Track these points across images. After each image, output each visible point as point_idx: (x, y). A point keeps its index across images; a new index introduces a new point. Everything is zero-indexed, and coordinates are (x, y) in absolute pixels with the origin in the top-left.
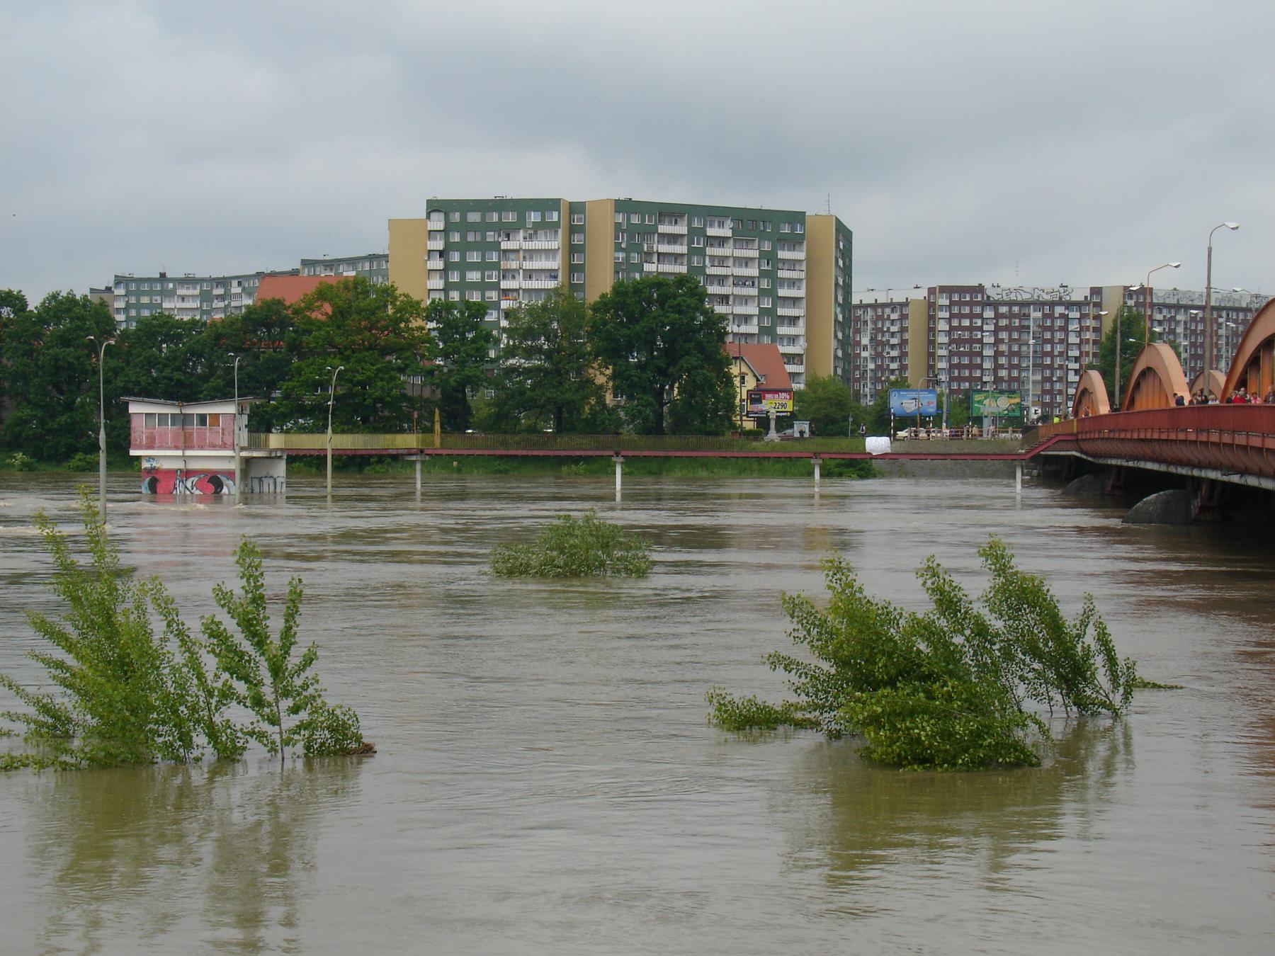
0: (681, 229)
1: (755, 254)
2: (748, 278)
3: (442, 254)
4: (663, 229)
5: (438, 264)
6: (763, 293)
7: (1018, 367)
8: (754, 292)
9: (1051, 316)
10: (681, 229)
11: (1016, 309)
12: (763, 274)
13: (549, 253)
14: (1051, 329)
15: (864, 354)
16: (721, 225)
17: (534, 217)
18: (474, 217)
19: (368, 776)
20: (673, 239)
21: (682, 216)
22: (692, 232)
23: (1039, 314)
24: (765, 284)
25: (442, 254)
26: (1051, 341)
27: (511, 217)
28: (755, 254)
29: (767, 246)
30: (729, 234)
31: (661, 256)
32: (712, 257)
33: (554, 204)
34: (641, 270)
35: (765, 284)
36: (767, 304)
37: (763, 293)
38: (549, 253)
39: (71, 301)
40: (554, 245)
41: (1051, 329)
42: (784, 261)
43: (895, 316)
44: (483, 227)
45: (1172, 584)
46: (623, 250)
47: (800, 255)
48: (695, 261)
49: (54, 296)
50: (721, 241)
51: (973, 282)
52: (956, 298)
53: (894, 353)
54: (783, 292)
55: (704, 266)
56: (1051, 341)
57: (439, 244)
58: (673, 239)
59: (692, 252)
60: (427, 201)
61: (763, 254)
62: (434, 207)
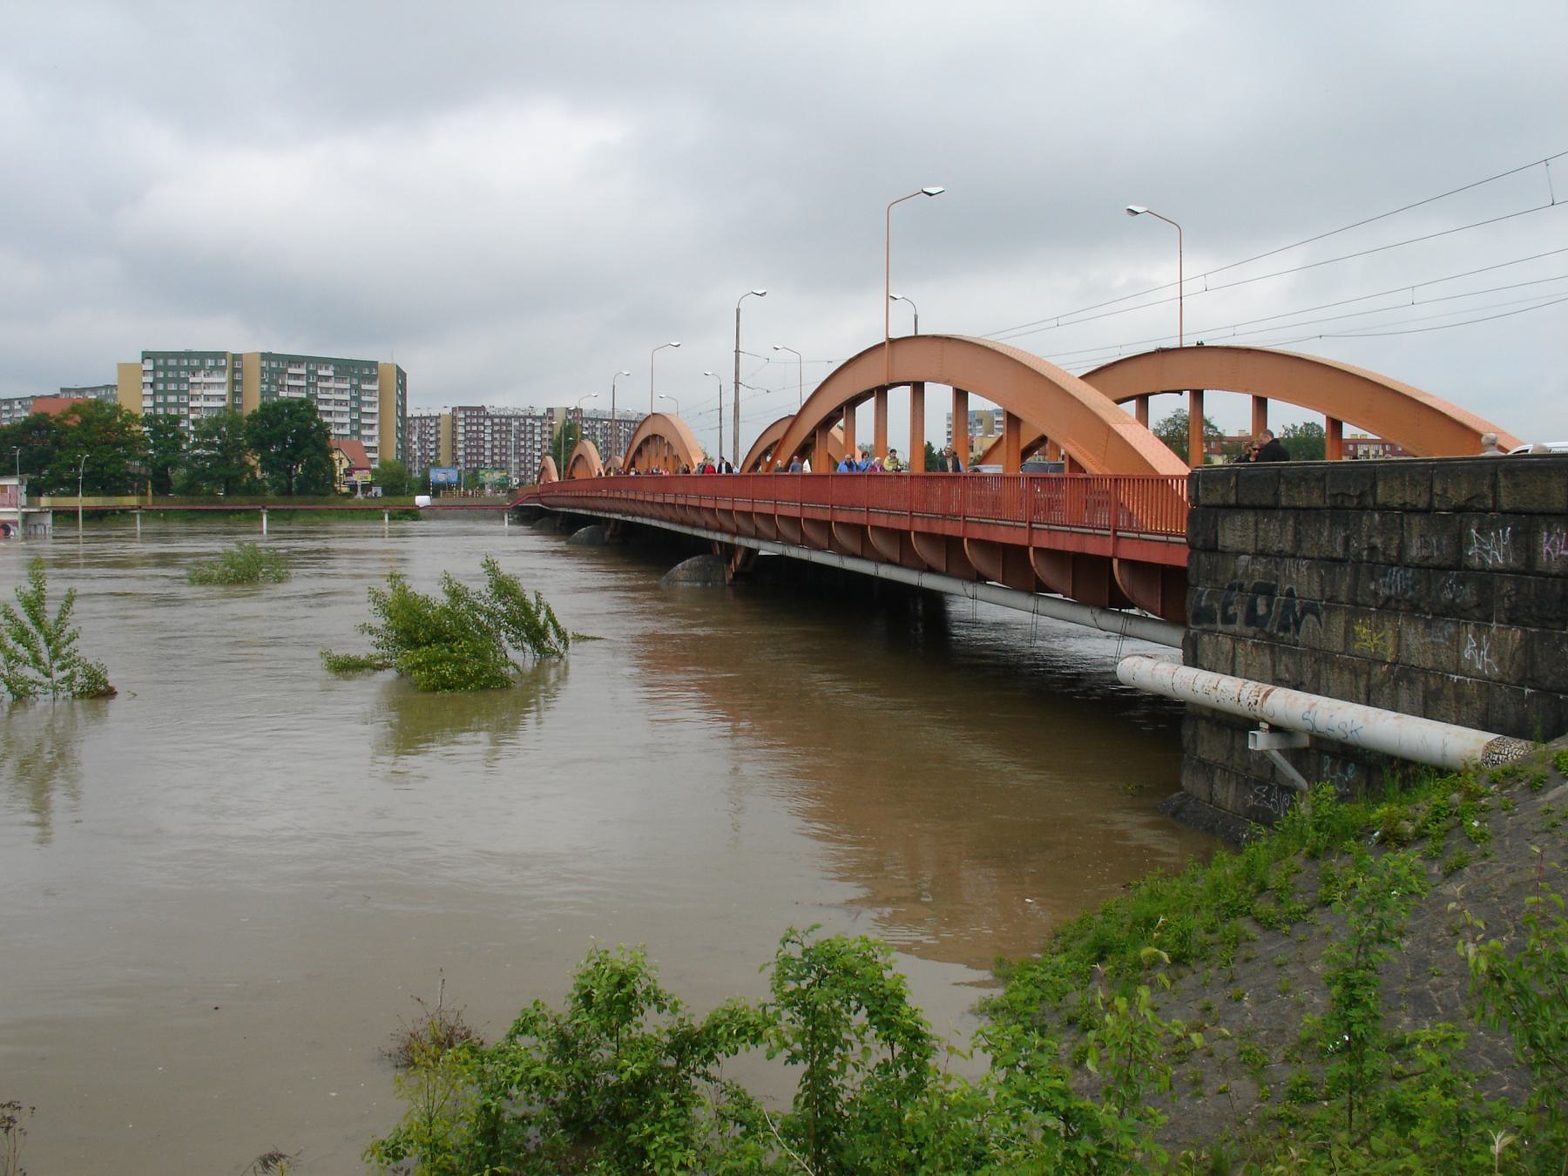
0: (303, 371)
1: (348, 386)
3: (152, 385)
4: (291, 370)
7: (505, 454)
8: (348, 409)
10: (303, 371)
12: (353, 398)
13: (220, 385)
15: (414, 447)
16: (327, 369)
17: (210, 363)
20: (298, 376)
21: (303, 363)
23: (517, 423)
24: (354, 405)
25: (152, 385)
27: (196, 363)
28: (348, 386)
29: (355, 382)
33: (223, 355)
36: (355, 417)
38: (220, 385)
41: (524, 432)
47: (375, 387)
48: (311, 391)
50: (327, 378)
53: (432, 446)
57: (150, 379)
58: (298, 376)
61: (352, 386)
62: (147, 356)
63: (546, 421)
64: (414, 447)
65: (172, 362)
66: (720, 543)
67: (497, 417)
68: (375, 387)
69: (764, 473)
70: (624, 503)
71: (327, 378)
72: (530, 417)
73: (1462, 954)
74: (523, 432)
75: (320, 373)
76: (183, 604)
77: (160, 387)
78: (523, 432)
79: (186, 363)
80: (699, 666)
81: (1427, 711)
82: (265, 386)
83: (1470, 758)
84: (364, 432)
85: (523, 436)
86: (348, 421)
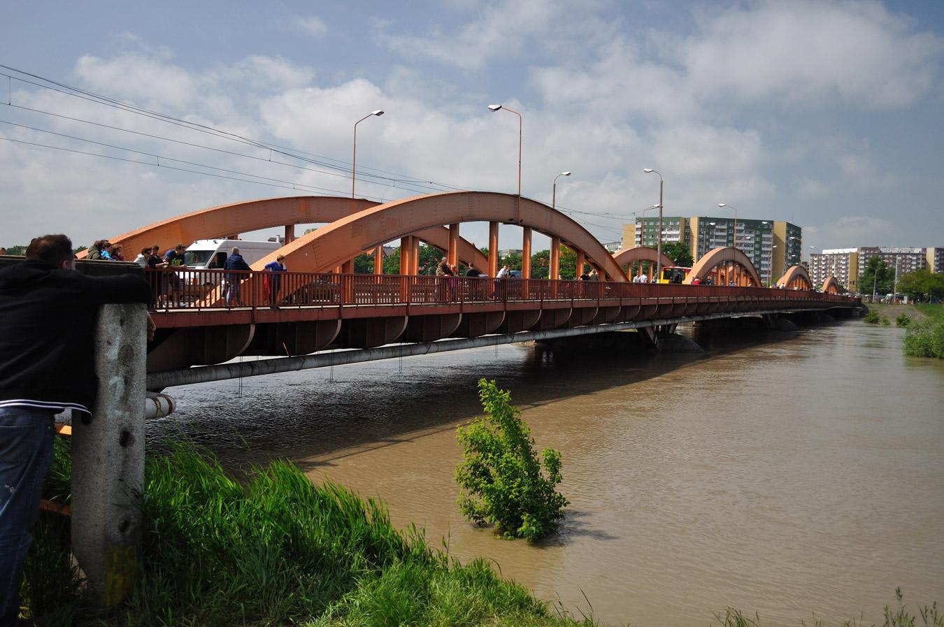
0: (725, 227)
2: (751, 244)
3: (641, 236)
5: (639, 239)
6: (756, 249)
8: (752, 249)
9: (905, 259)
10: (725, 227)
11: (891, 256)
12: (756, 242)
13: (676, 236)
14: (905, 264)
15: (833, 272)
16: (741, 225)
18: (652, 224)
20: (722, 230)
21: (725, 222)
22: (729, 228)
23: (900, 258)
24: (757, 246)
25: (641, 236)
26: (905, 268)
29: (758, 233)
31: (717, 237)
32: (737, 237)
35: (757, 246)
36: (758, 253)
37: (756, 249)
38: (676, 236)
40: (678, 232)
41: (905, 264)
42: (765, 238)
43: (844, 258)
45: (632, 324)
47: (771, 236)
48: (730, 238)
49: (33, 239)
50: (740, 231)
53: (843, 272)
54: (763, 249)
55: (733, 240)
56: (905, 268)
57: (639, 233)
58: (722, 230)
59: (729, 235)
61: (756, 236)
62: (639, 220)
63: (920, 257)
64: (833, 272)
65: (652, 224)
67: (887, 254)
68: (771, 236)
71: (740, 231)
72: (909, 254)
74: (903, 263)
76: (816, 344)
78: (903, 263)
80: (337, 338)
81: (268, 355)
82: (701, 236)
84: (763, 262)
85: (903, 266)
86: (753, 255)
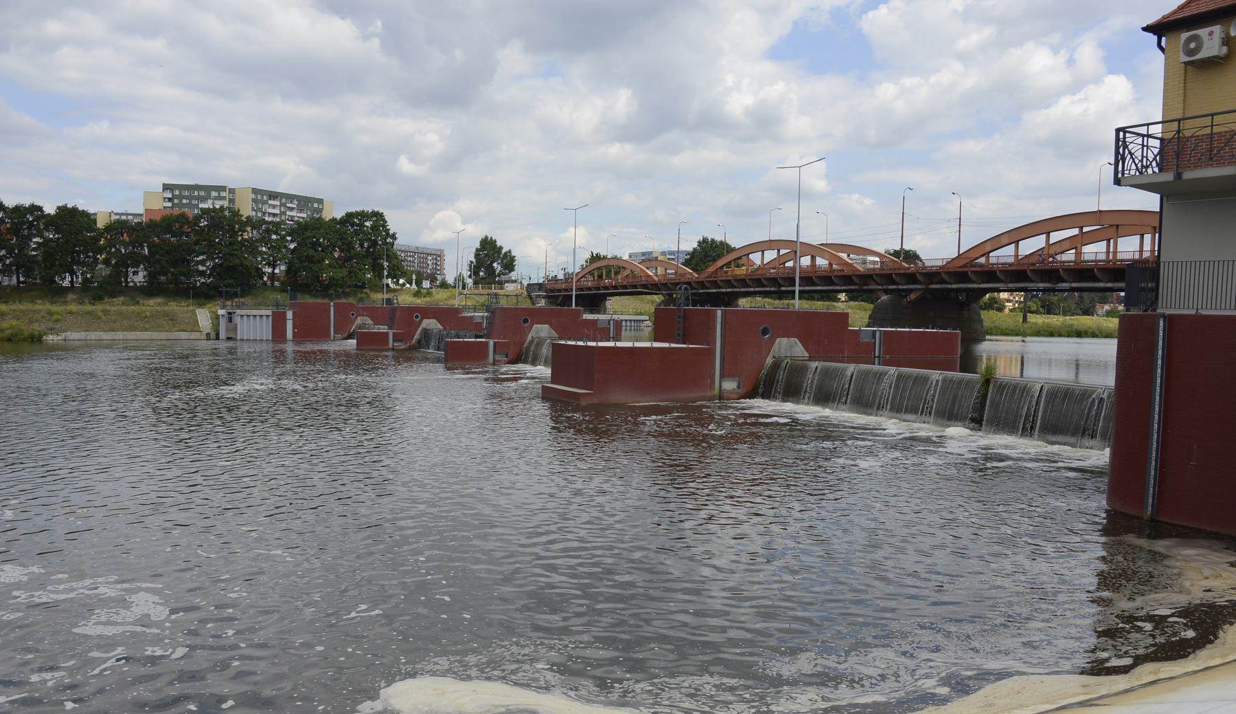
1: (278, 203)
4: (270, 202)
7: (631, 330)
17: (214, 194)
19: (505, 242)
20: (274, 207)
21: (277, 197)
27: (202, 193)
28: (278, 203)
30: (295, 206)
33: (223, 188)
34: (198, 207)
39: (22, 206)
44: (190, 198)
46: (255, 210)
50: (291, 209)
51: (1114, 134)
52: (177, 193)
58: (274, 207)
60: (442, 251)
62: (166, 187)
66: (1064, 281)
69: (1203, 32)
70: (1059, 441)
73: (48, 588)
75: (288, 205)
77: (176, 201)
79: (196, 193)
83: (1090, 328)
